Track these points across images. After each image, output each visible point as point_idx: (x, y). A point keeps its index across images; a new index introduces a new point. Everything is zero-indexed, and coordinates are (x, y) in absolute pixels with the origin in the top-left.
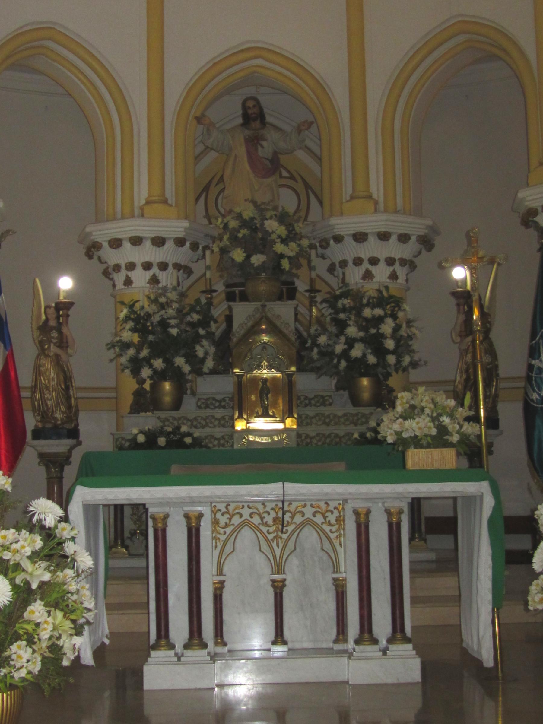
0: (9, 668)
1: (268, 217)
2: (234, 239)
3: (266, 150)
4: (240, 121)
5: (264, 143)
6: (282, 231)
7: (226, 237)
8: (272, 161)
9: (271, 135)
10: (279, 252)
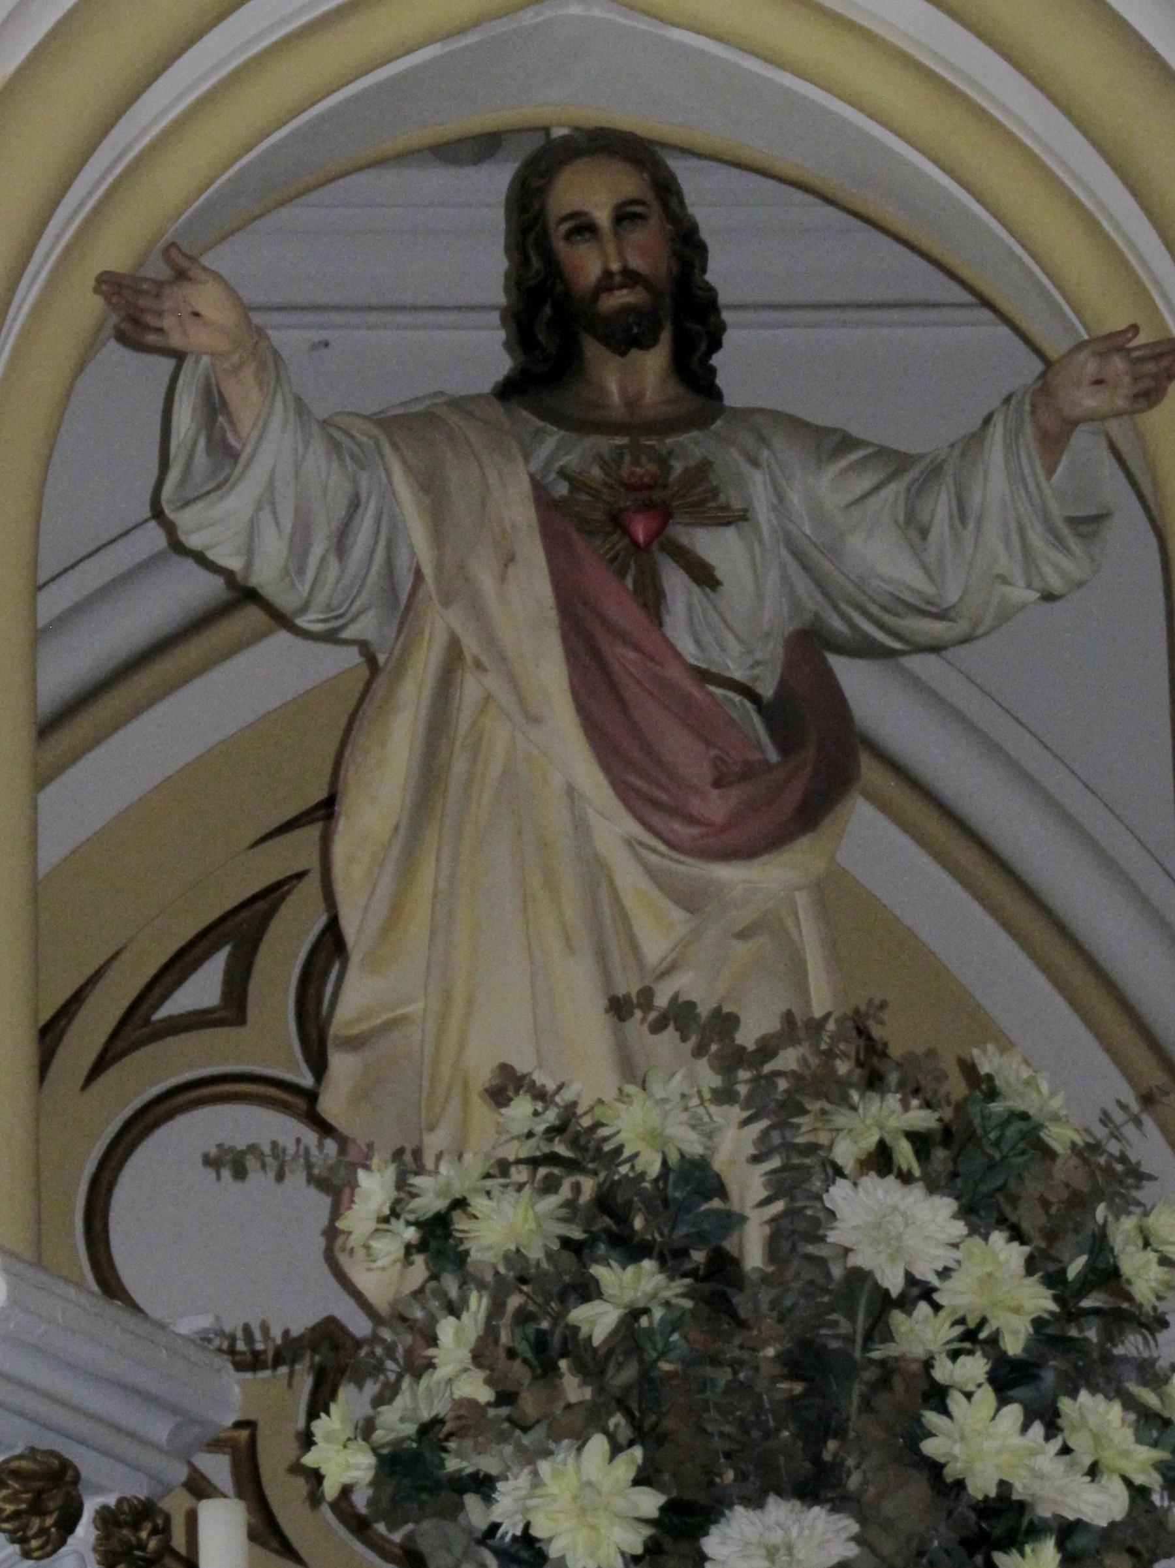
0: (654, 497)
1: (845, 1153)
2: (536, 1350)
3: (730, 613)
4: (488, 356)
5: (716, 546)
6: (1001, 1285)
7: (455, 1339)
8: (780, 715)
9: (787, 493)
10: (982, 1485)
